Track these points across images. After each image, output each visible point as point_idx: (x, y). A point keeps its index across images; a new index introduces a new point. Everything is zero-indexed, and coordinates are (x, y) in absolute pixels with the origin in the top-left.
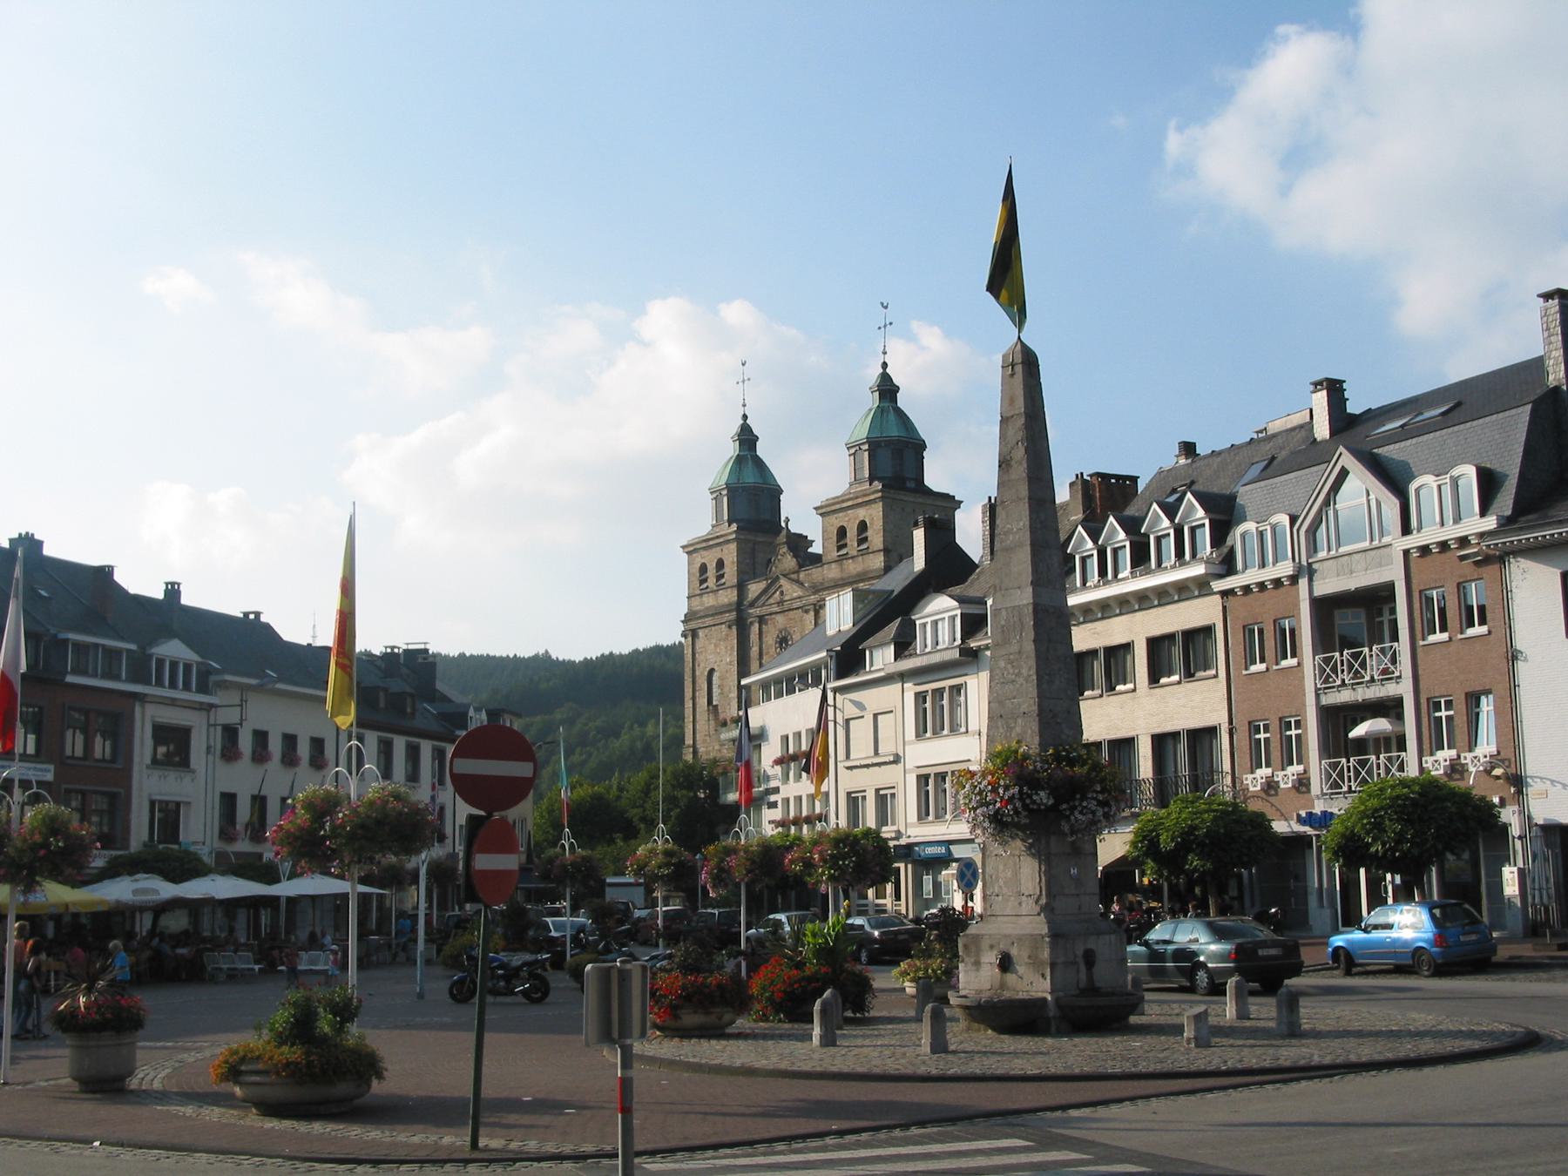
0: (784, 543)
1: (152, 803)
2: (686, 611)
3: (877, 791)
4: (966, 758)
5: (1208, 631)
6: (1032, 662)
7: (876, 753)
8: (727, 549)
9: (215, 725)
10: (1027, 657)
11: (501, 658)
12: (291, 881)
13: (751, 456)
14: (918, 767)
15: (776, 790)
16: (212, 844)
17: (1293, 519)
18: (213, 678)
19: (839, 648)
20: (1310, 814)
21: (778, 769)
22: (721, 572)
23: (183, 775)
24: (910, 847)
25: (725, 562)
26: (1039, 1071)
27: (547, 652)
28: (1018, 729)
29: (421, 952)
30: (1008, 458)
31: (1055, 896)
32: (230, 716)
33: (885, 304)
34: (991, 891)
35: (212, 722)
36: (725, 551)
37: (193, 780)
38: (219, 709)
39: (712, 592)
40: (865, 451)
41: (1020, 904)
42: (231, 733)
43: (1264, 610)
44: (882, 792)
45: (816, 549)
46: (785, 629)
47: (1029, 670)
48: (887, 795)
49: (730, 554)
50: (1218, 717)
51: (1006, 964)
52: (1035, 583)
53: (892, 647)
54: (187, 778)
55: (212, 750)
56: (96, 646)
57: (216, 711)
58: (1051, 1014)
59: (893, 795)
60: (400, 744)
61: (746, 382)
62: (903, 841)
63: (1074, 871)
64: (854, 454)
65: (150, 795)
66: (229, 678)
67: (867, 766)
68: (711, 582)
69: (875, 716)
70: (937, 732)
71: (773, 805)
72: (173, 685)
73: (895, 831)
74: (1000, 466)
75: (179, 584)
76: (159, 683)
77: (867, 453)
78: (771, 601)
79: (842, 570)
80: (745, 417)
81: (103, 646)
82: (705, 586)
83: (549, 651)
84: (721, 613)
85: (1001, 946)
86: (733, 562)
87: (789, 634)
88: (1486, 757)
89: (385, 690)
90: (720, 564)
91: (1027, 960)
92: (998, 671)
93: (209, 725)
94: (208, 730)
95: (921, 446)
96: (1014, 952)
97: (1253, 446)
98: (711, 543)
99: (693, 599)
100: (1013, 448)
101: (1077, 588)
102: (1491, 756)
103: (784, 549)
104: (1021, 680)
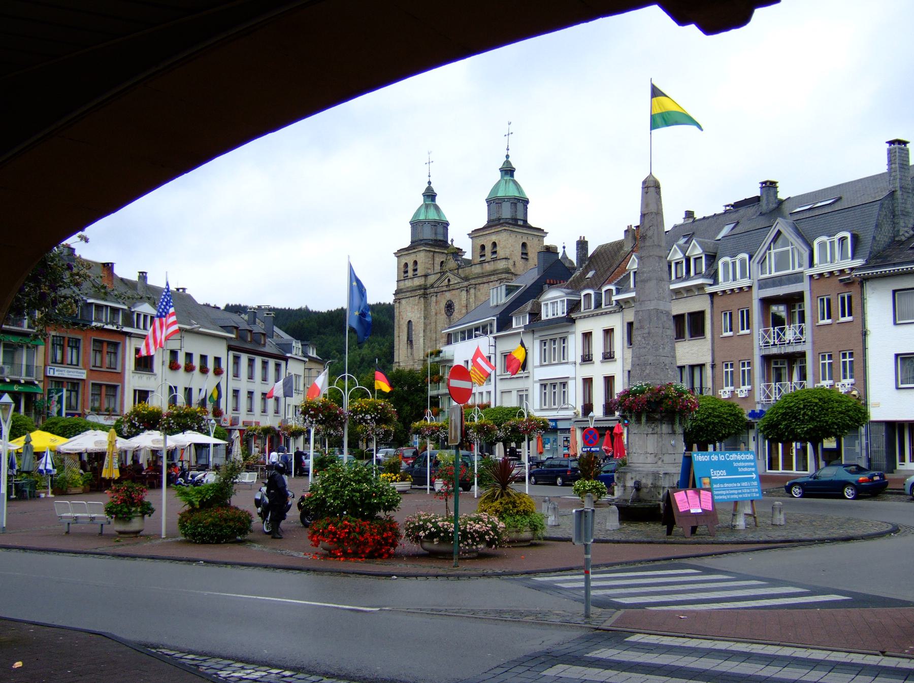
1: (135, 391)
5: (702, 313)
11: (281, 309)
17: (750, 258)
20: (753, 411)
27: (306, 306)
30: (644, 235)
36: (418, 257)
37: (155, 379)
41: (647, 458)
42: (174, 353)
43: (734, 304)
45: (468, 256)
46: (450, 301)
50: (707, 359)
54: (153, 378)
56: (107, 306)
59: (527, 395)
60: (244, 359)
61: (431, 163)
63: (673, 442)
68: (410, 274)
72: (138, 327)
75: (146, 273)
76: (138, 327)
78: (443, 284)
79: (482, 268)
80: (429, 183)
81: (110, 306)
84: (415, 290)
87: (452, 303)
88: (848, 385)
89: (250, 331)
97: (726, 214)
102: (852, 384)
104: (649, 347)
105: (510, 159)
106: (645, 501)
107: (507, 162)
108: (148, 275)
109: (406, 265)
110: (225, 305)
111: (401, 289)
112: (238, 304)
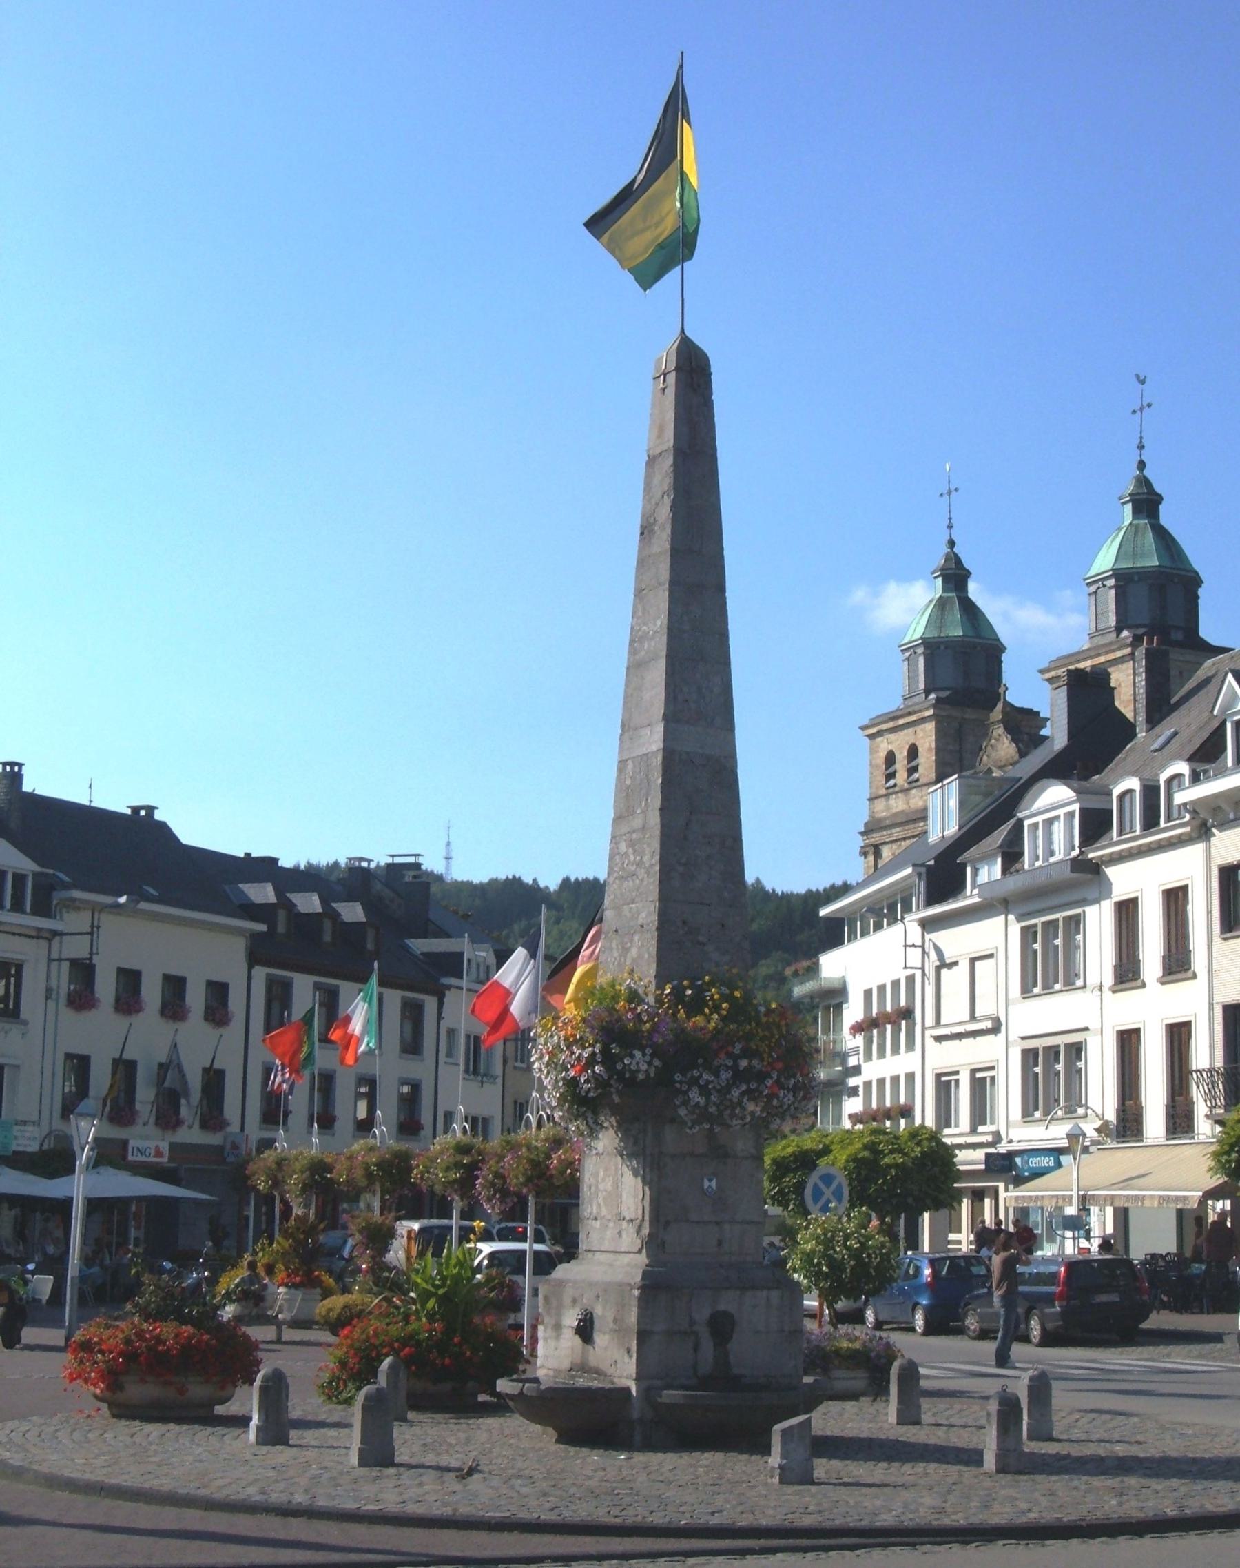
0: (998, 722)
2: (866, 819)
3: (973, 1071)
4: (1082, 1026)
6: (656, 845)
7: (973, 1018)
8: (922, 730)
9: (60, 960)
10: (651, 836)
13: (959, 598)
14: (1023, 1038)
15: (857, 1070)
16: (51, 1123)
18: (57, 896)
19: (932, 862)
21: (859, 1040)
22: (914, 764)
23: (7, 1026)
24: (1010, 1155)
25: (920, 749)
26: (356, 1506)
28: (634, 952)
29: (72, 1278)
31: (667, 1223)
32: (77, 948)
33: (1142, 378)
34: (589, 1211)
35: (55, 955)
36: (920, 734)
38: (64, 937)
39: (901, 791)
40: (1111, 588)
41: (620, 1233)
42: (84, 971)
44: (979, 1075)
47: (652, 857)
48: (985, 1078)
49: (926, 737)
51: (585, 1331)
52: (670, 719)
53: (999, 860)
54: (15, 1030)
55: (54, 996)
57: (61, 943)
58: (635, 1415)
62: (1002, 1148)
63: (710, 1184)
64: (1095, 593)
66: (77, 894)
67: (959, 1036)
68: (901, 778)
69: (973, 961)
70: (1048, 988)
71: (854, 1092)
73: (992, 1133)
74: (642, 534)
75: (20, 765)
77: (1113, 592)
82: (891, 782)
83: (761, 879)
85: (585, 1301)
86: (930, 749)
90: (913, 752)
91: (611, 1325)
92: (617, 858)
93: (50, 960)
94: (48, 966)
95: (1192, 582)
96: (598, 1311)
98: (901, 722)
99: (876, 801)
100: (657, 504)
101: (1226, 768)
103: (999, 730)
105: (1146, 472)
106: (598, 1372)
107: (1144, 482)
108: (24, 770)
109: (890, 759)
110: (559, 881)
111: (880, 820)
112: (591, 878)
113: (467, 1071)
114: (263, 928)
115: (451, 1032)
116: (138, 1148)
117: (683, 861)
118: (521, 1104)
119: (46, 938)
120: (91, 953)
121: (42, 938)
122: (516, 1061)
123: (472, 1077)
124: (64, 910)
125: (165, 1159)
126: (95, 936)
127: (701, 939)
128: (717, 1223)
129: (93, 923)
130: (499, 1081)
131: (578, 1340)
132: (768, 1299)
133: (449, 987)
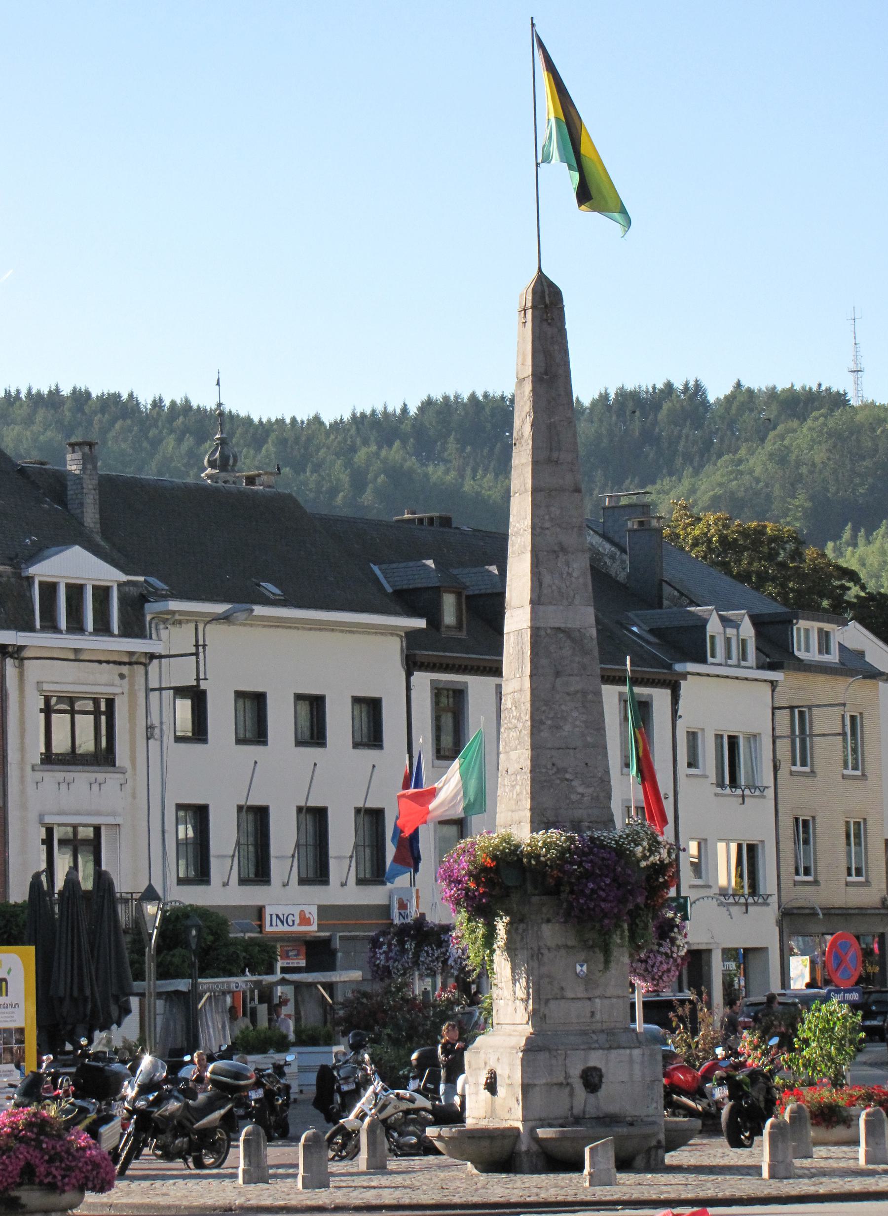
9: (160, 689)
12: (445, 922)
18: (151, 609)
23: (100, 777)
31: (547, 1001)
35: (154, 684)
55: (157, 732)
58: (524, 1148)
65: (41, 817)
66: (174, 605)
76: (51, 625)
93: (148, 690)
113: (721, 784)
114: (421, 623)
115: (692, 736)
116: (277, 916)
117: (551, 716)
118: (805, 822)
119: (141, 663)
120: (198, 679)
121: (137, 663)
122: (794, 764)
123: (728, 791)
124: (162, 626)
125: (314, 927)
126: (201, 655)
127: (568, 776)
128: (590, 999)
129: (197, 641)
130: (770, 793)
131: (488, 1094)
132: (631, 1055)
133: (684, 675)
